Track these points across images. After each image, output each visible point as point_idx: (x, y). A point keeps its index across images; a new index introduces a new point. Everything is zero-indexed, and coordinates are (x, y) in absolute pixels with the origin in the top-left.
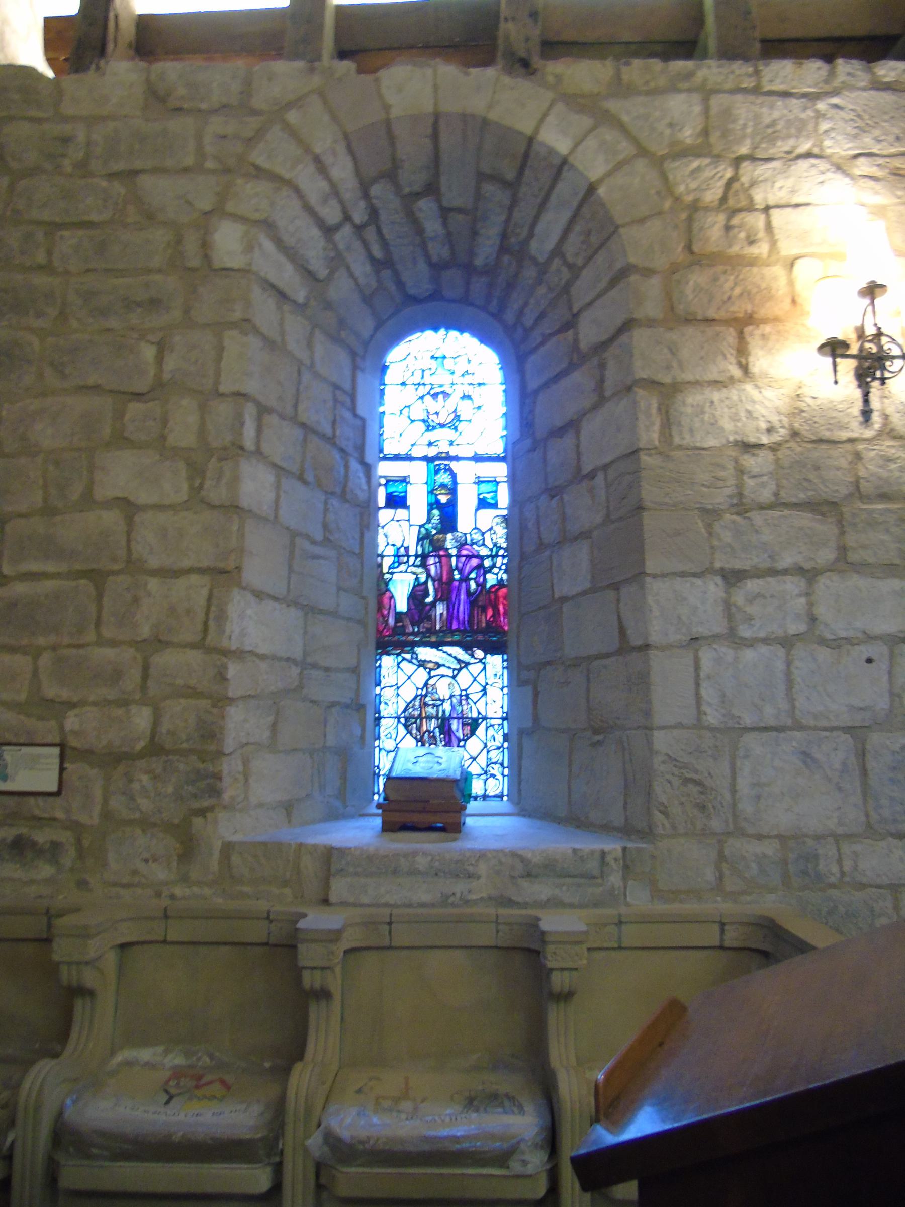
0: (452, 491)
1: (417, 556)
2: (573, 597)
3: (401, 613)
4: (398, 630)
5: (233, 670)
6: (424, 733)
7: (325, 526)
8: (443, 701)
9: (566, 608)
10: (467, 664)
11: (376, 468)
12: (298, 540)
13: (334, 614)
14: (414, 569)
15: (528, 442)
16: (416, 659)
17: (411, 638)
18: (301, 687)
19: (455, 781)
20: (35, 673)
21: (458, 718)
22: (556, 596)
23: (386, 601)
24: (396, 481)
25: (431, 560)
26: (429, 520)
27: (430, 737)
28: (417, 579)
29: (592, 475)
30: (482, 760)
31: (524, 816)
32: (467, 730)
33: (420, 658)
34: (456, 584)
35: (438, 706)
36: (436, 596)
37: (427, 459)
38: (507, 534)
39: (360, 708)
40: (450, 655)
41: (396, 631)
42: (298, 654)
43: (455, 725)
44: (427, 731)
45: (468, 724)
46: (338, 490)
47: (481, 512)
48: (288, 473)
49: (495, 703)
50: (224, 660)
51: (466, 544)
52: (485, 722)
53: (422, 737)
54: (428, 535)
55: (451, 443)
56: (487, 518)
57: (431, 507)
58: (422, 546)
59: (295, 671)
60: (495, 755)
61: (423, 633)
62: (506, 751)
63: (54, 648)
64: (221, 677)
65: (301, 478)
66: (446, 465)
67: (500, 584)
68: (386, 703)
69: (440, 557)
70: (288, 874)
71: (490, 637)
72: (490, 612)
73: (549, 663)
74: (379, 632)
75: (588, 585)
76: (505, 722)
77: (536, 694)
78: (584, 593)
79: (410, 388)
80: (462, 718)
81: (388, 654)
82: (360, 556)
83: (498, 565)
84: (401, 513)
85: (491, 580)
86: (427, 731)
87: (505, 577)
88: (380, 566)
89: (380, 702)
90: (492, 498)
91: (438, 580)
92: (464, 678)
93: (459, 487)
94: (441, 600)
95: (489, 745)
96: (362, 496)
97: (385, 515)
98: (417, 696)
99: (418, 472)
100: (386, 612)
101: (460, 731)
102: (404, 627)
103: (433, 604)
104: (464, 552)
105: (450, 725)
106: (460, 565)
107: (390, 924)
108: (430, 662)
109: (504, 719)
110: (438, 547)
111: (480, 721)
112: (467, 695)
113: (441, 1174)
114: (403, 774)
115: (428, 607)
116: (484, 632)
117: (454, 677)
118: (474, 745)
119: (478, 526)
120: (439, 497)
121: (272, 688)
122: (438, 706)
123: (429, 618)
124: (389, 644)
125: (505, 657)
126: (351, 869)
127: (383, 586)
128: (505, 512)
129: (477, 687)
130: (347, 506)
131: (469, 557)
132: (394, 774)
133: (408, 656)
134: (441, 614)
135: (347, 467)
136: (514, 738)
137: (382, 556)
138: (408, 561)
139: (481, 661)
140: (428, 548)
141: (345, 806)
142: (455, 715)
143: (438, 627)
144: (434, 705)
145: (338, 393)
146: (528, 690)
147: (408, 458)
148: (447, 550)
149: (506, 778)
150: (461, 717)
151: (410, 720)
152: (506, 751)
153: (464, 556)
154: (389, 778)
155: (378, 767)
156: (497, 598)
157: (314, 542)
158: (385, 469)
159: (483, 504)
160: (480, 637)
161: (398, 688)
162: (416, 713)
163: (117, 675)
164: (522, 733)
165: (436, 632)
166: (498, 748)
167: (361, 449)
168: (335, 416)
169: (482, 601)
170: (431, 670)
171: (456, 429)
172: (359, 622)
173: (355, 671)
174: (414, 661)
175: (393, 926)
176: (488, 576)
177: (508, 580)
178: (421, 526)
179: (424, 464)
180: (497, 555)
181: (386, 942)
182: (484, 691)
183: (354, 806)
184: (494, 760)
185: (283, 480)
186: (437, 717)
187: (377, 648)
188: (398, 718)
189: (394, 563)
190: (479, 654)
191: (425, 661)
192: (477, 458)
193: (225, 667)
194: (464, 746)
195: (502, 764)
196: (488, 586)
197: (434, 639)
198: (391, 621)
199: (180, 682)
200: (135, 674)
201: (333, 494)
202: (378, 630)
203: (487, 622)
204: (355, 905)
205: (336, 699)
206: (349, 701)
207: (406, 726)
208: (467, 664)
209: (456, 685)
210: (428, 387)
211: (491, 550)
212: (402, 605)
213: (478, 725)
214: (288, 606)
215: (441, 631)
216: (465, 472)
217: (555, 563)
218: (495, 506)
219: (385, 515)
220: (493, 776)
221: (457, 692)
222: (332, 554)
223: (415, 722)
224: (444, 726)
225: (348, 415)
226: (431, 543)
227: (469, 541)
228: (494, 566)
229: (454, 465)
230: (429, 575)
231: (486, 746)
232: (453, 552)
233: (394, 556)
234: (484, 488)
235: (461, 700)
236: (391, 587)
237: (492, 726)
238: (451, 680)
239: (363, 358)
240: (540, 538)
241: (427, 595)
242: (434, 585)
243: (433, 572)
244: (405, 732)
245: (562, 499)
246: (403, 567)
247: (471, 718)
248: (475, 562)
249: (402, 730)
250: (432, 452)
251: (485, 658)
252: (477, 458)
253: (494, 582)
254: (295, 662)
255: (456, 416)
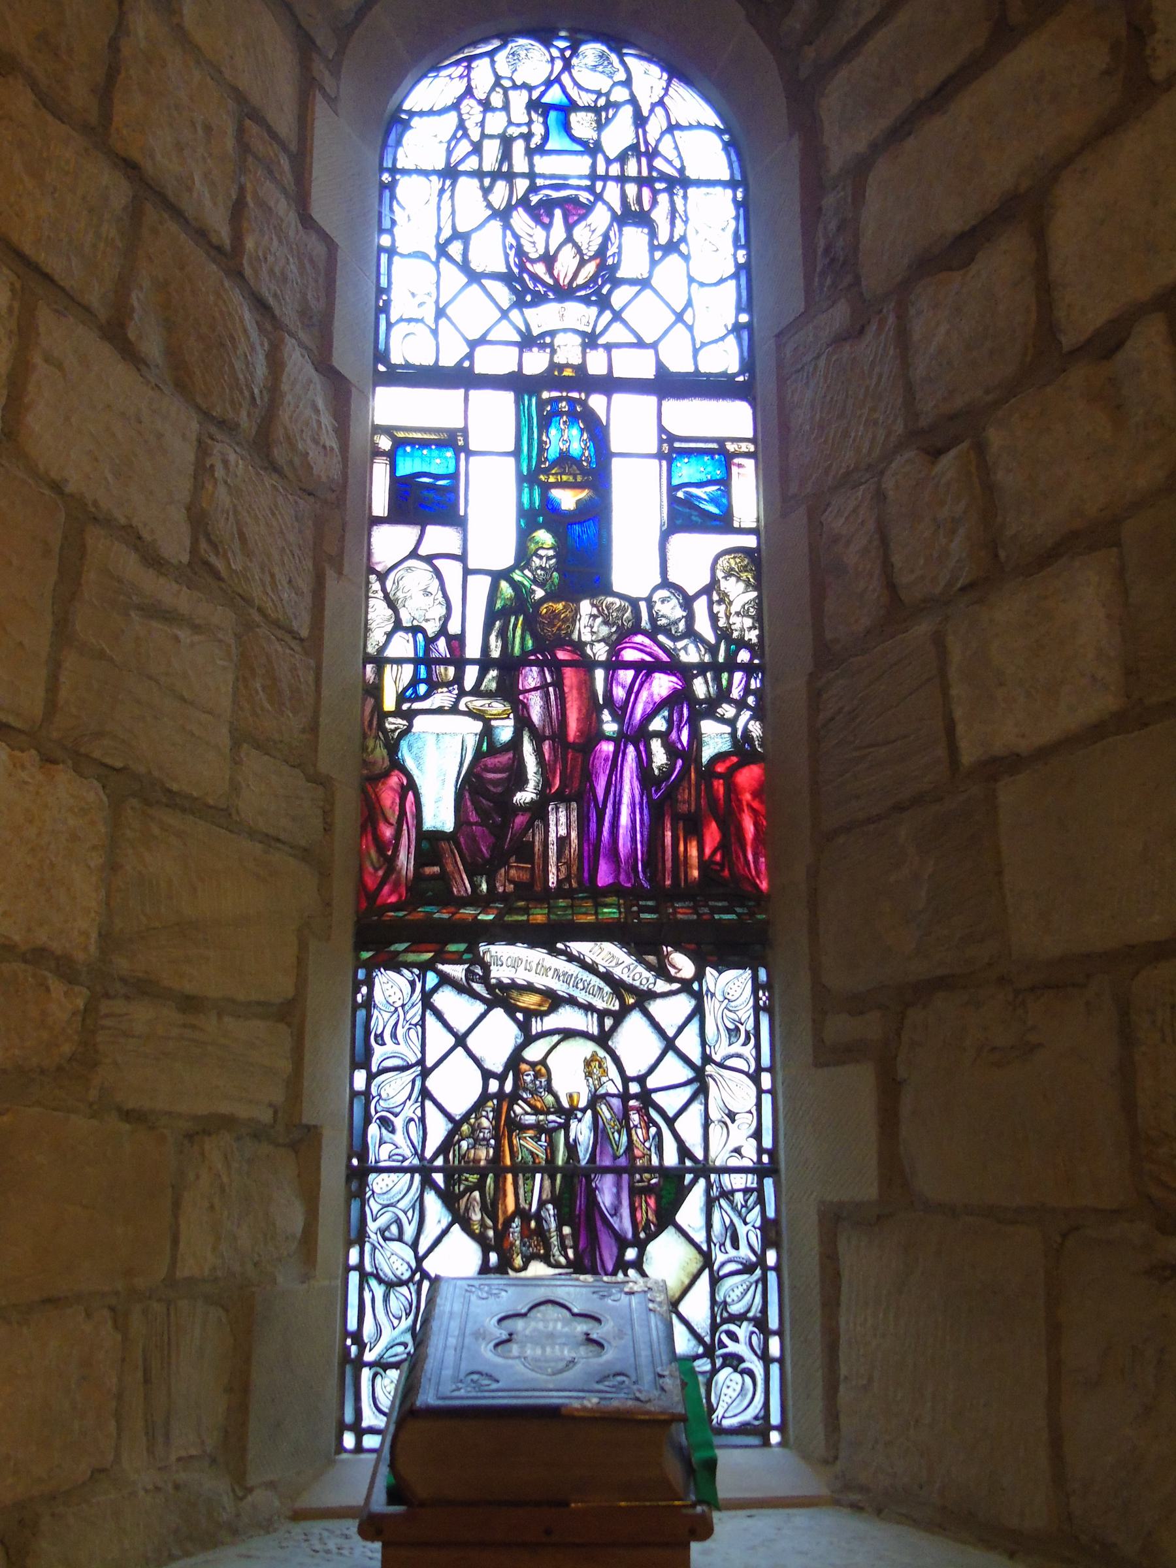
0: (595, 473)
1: (485, 663)
2: (1043, 753)
3: (437, 836)
4: (428, 888)
6: (509, 1221)
7: (198, 521)
8: (569, 1113)
9: (1010, 793)
10: (643, 997)
11: (366, 399)
12: (97, 541)
13: (222, 815)
14: (478, 703)
15: (839, 315)
16: (485, 979)
17: (469, 911)
19: (663, 1423)
21: (617, 1171)
22: (968, 757)
23: (388, 798)
24: (424, 444)
25: (531, 677)
26: (523, 557)
27: (526, 1233)
28: (488, 732)
29: (1108, 342)
30: (697, 1308)
31: (856, 1507)
32: (648, 1209)
33: (496, 973)
34: (608, 748)
35: (550, 1132)
36: (546, 782)
37: (517, 383)
38: (759, 603)
39: (303, 1141)
40: (591, 968)
41: (420, 890)
42: (76, 928)
43: (606, 1193)
44: (519, 1212)
45: (648, 1190)
46: (246, 422)
47: (679, 541)
48: (71, 303)
49: (731, 1123)
51: (637, 630)
52: (702, 1182)
53: (502, 1235)
54: (521, 603)
55: (590, 340)
56: (694, 558)
57: (529, 521)
58: (503, 634)
60: (738, 1292)
61: (504, 898)
62: (772, 1277)
65: (115, 333)
66: (571, 401)
67: (743, 750)
68: (385, 1123)
69: (557, 667)
71: (715, 910)
72: (712, 834)
73: (943, 983)
74: (367, 896)
75: (1106, 703)
76: (768, 1183)
77: (890, 1089)
78: (1097, 731)
79: (468, 187)
80: (631, 1169)
81: (395, 965)
82: (313, 645)
83: (736, 694)
84: (440, 538)
85: (715, 738)
86: (519, 1212)
87: (756, 729)
88: (376, 691)
89: (367, 1120)
90: (713, 500)
91: (552, 733)
92: (635, 1042)
93: (617, 466)
94: (562, 798)
95: (719, 1257)
96: (324, 467)
97: (389, 543)
98: (485, 1097)
99: (493, 419)
100: (388, 832)
101: (625, 1211)
102: (444, 878)
103: (538, 811)
104: (630, 655)
105: (591, 1195)
106: (619, 693)
108: (530, 988)
109: (760, 1171)
110: (552, 646)
111: (689, 1178)
112: (646, 1097)
114: (465, 1396)
115: (520, 820)
116: (694, 893)
117: (603, 1039)
118: (668, 1259)
119: (672, 578)
120: (556, 493)
122: (550, 1132)
123: (524, 851)
124: (400, 931)
125: (763, 974)
127: (381, 753)
128: (751, 541)
129: (673, 1070)
130: (270, 480)
131: (645, 670)
132: (428, 1397)
133: (457, 971)
134: (563, 841)
135: (275, 363)
136: (806, 1234)
137: (380, 661)
138: (459, 679)
139: (686, 986)
140: (520, 641)
141: (241, 1485)
142: (607, 1162)
143: (552, 879)
144: (539, 1128)
145: (253, 128)
146: (861, 1079)
147: (461, 377)
148: (579, 646)
149: (775, 1369)
150: (628, 1168)
151: (462, 1178)
152: (772, 1277)
153: (628, 665)
154: (408, 1413)
155: (357, 1337)
156: (732, 789)
157: (154, 561)
158: (392, 407)
159: (684, 515)
160: (683, 912)
161: (426, 1073)
162: (483, 1154)
164: (834, 1220)
165: (546, 896)
166: (748, 1269)
167: (321, 327)
168: (242, 189)
169: (687, 799)
170: (530, 1014)
171: (604, 303)
172: (305, 854)
173: (289, 1013)
174: (478, 988)
176: (708, 727)
177: (763, 741)
178: (498, 576)
179: (507, 398)
180: (732, 666)
182: (700, 1085)
183: (271, 1485)
184: (735, 1309)
185: (45, 316)
186: (550, 1169)
187: (360, 946)
188: (424, 1171)
189: (415, 682)
190: (683, 965)
191: (514, 986)
192: (667, 385)
194: (638, 1264)
195: (761, 1323)
196: (707, 754)
197: (539, 916)
198: (405, 860)
201: (227, 426)
202: (362, 883)
203: (703, 865)
205: (224, 1108)
206: (266, 1116)
207: (449, 1199)
208: (643, 997)
209: (610, 1064)
210: (522, 185)
211: (713, 650)
212: (439, 813)
213: (682, 1193)
214: (48, 760)
215: (560, 892)
216: (631, 422)
217: (956, 655)
218: (723, 523)
219: (389, 543)
220: (733, 1361)
221: (612, 1085)
222: (221, 616)
223: (480, 1186)
224: (564, 1194)
225: (283, 207)
226: (529, 627)
227: (645, 623)
228: (723, 695)
229: (597, 402)
230: (523, 722)
231: (707, 1260)
232: (600, 652)
233: (416, 661)
234: (688, 471)
235: (626, 1110)
236: (406, 754)
237: (728, 1195)
238: (587, 1048)
239: (335, 68)
240: (891, 586)
241: (520, 781)
242: (539, 752)
243: (536, 713)
244: (446, 1219)
245: (980, 448)
246: (442, 698)
247: (662, 1170)
248: (662, 685)
249: (436, 1212)
250: (535, 363)
251: (699, 976)
252: (667, 385)
253: (724, 745)
254: (65, 968)
255: (602, 267)
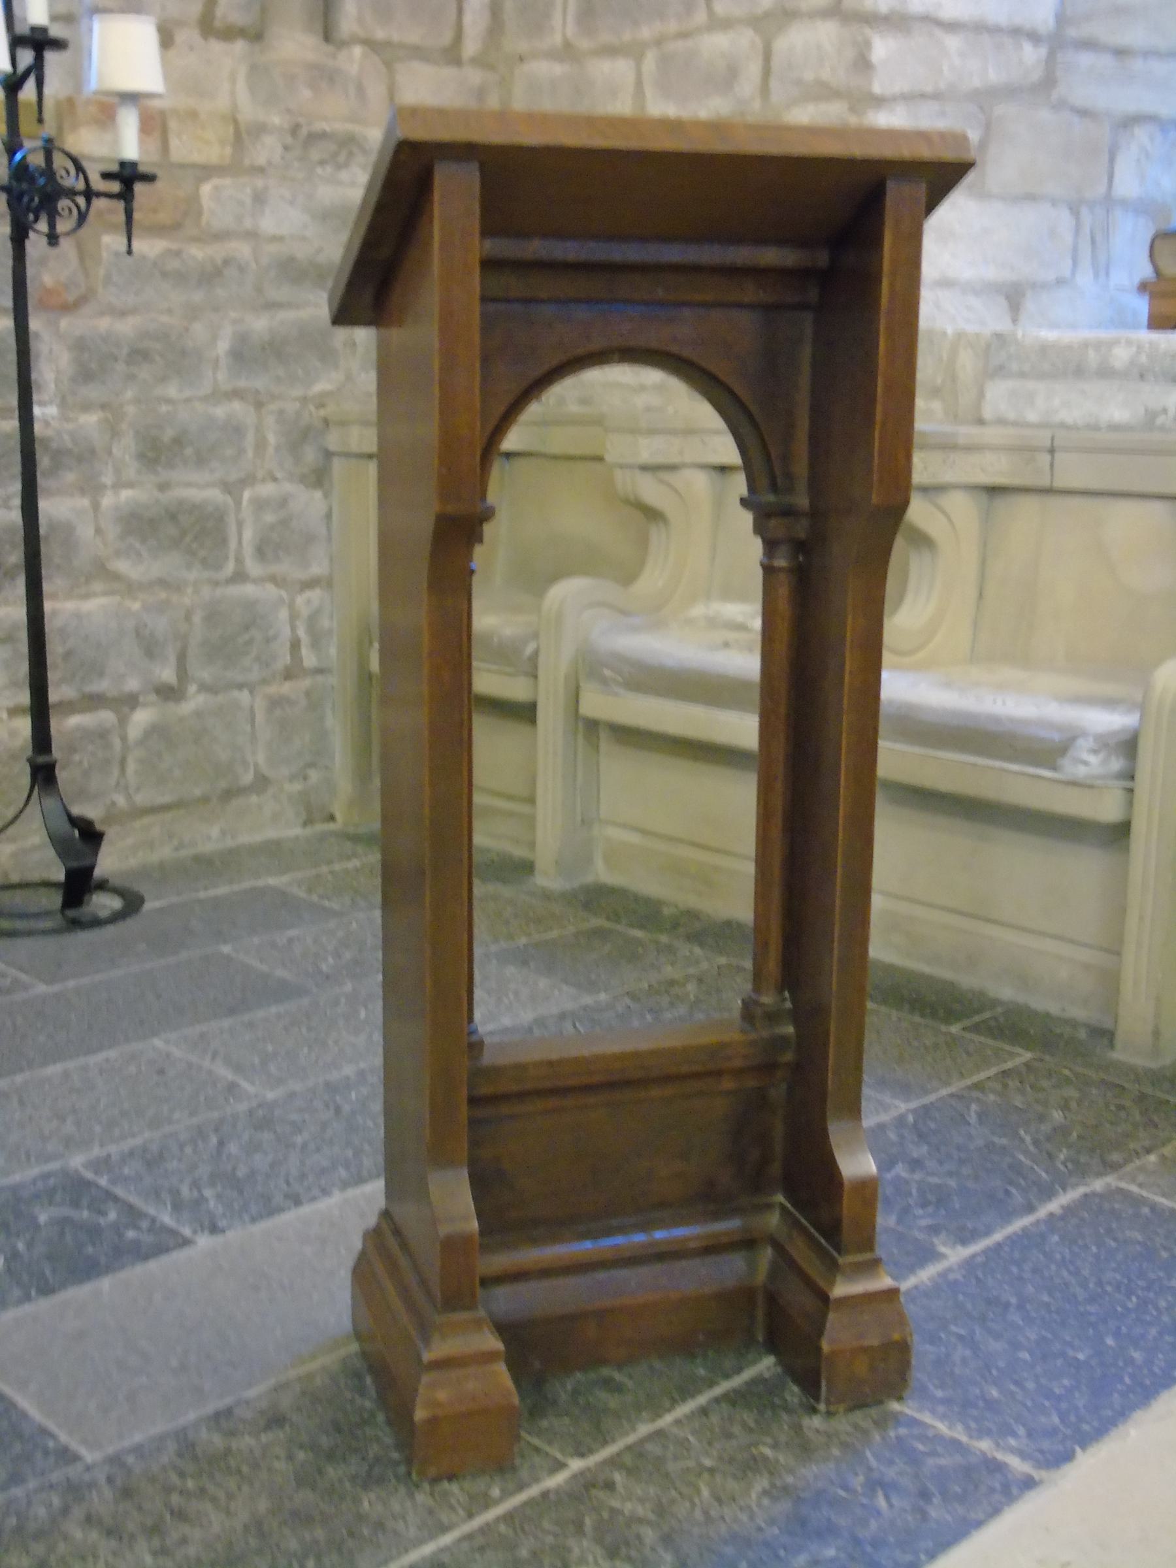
5: (882, 48)
18: (1048, 81)
20: (639, 83)
50: (867, 31)
59: (1032, 54)
63: (659, 42)
64: (863, 64)
70: (939, 381)
107: (1052, 451)
113: (974, 765)
121: (977, 82)
126: (1014, 367)
163: (732, 74)
175: (1057, 456)
181: (1045, 482)
193: (868, 44)
199: (809, 76)
200: (753, 70)
204: (1015, 424)
254: (1034, 37)
